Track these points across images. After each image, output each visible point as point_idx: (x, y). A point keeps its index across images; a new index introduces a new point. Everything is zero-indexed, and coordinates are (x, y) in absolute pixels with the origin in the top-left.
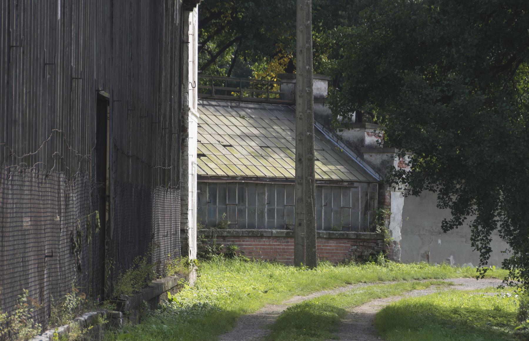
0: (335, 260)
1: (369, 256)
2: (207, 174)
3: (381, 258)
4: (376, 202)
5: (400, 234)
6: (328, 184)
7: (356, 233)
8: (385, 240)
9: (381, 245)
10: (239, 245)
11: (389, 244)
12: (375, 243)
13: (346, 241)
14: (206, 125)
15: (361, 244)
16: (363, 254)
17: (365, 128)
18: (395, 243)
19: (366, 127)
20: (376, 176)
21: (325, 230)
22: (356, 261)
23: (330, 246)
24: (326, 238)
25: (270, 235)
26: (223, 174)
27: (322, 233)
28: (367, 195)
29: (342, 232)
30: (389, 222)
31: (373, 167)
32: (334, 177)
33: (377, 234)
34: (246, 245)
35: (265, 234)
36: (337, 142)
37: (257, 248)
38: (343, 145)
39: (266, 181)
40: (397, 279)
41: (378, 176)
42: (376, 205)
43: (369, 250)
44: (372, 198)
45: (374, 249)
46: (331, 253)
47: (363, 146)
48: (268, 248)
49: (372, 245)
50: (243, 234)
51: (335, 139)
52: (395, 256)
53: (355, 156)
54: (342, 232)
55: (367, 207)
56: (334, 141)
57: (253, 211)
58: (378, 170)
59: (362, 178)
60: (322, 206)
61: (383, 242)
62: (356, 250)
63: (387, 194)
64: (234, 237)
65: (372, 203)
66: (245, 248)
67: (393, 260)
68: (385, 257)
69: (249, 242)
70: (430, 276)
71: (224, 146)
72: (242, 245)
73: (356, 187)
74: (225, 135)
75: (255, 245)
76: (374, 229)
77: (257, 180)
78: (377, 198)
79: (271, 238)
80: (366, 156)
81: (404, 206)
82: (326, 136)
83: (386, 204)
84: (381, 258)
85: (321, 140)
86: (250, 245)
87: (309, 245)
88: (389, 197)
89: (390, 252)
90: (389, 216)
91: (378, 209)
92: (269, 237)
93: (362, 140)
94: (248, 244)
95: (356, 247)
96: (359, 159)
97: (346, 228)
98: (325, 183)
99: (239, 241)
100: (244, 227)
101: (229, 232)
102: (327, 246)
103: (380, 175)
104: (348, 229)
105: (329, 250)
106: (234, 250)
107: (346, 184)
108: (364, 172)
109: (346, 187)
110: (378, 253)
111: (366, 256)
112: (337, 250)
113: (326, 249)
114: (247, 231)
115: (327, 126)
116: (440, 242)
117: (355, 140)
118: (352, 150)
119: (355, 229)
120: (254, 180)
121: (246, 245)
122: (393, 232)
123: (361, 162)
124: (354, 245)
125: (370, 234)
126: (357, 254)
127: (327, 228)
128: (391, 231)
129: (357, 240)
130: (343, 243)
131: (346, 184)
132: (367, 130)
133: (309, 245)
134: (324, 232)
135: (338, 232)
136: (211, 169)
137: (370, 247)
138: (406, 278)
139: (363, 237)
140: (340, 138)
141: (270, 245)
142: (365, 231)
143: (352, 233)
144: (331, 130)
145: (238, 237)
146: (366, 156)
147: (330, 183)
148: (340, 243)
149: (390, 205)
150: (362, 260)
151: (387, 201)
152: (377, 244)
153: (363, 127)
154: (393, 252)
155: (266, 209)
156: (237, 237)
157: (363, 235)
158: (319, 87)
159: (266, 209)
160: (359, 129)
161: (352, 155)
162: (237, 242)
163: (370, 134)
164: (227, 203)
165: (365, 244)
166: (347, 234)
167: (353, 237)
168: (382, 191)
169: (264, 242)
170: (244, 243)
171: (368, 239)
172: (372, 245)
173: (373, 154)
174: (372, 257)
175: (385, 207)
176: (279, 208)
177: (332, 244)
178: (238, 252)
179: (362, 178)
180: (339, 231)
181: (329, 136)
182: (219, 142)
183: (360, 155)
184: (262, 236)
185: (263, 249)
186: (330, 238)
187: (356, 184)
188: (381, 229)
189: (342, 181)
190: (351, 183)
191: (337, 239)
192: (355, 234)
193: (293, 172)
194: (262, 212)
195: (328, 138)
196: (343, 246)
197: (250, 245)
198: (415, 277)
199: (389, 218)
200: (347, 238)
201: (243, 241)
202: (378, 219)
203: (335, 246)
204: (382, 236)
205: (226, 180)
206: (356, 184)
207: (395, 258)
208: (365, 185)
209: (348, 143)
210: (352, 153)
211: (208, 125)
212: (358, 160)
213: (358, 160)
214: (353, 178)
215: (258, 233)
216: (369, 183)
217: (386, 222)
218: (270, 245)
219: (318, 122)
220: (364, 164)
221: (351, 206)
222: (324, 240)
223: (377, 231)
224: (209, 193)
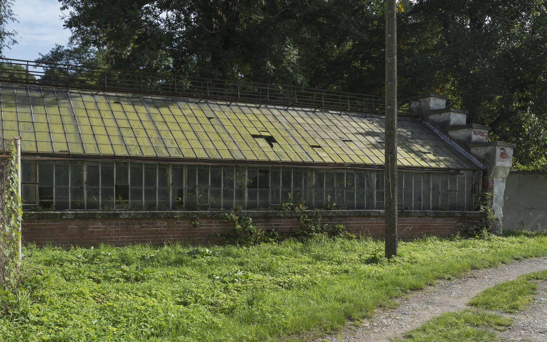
0: (442, 234)
1: (473, 231)
2: (314, 161)
3: (485, 232)
4: (481, 186)
5: (502, 212)
6: (435, 171)
7: (462, 212)
8: (488, 217)
9: (484, 221)
10: (344, 224)
11: (492, 221)
12: (479, 220)
13: (452, 219)
14: (335, 127)
15: (466, 221)
16: (468, 229)
17: (472, 128)
18: (497, 219)
19: (473, 127)
20: (481, 166)
21: (433, 209)
22: (462, 235)
23: (437, 223)
24: (433, 217)
25: (378, 215)
26: (331, 161)
27: (429, 212)
28: (472, 181)
29: (448, 211)
30: (492, 203)
31: (479, 159)
32: (442, 166)
33: (481, 213)
34: (353, 224)
35: (372, 214)
36: (450, 142)
37: (364, 226)
38: (454, 143)
39: (375, 168)
40: (494, 264)
41: (482, 166)
42: (480, 189)
43: (473, 226)
44: (477, 183)
45: (478, 225)
46: (438, 229)
47: (470, 143)
48: (376, 226)
49: (476, 221)
50: (349, 214)
51: (449, 139)
52: (497, 230)
53: (464, 151)
54: (448, 211)
55: (473, 190)
56: (448, 140)
57: (362, 194)
58: (482, 161)
59: (467, 167)
60: (430, 190)
61: (487, 219)
62: (462, 226)
63: (490, 180)
64: (341, 217)
65: (477, 187)
66: (352, 227)
67: (495, 233)
68: (488, 232)
69: (356, 221)
70: (530, 254)
71: (344, 141)
72: (350, 224)
73: (462, 174)
74: (349, 134)
75: (362, 223)
76: (478, 209)
77: (366, 167)
78: (481, 183)
79: (379, 217)
80: (473, 150)
81: (505, 190)
82: (441, 137)
83: (489, 188)
84: (485, 232)
85: (437, 140)
86: (358, 223)
87: (388, 230)
88: (492, 182)
89: (492, 227)
90: (492, 197)
91: (483, 192)
92: (377, 217)
93: (470, 138)
94: (354, 222)
95: (461, 224)
96: (467, 153)
97: (453, 207)
98: (433, 170)
99: (346, 221)
100: (353, 208)
101: (334, 212)
102: (435, 223)
103: (484, 165)
104: (455, 209)
105: (437, 226)
106: (339, 228)
107: (452, 171)
108: (470, 162)
109: (452, 174)
110: (482, 228)
111: (471, 231)
112: (444, 226)
113: (432, 226)
114: (354, 211)
115: (442, 130)
116: (531, 214)
117: (464, 138)
118: (461, 147)
119: (461, 208)
120: (361, 167)
121: (353, 224)
122: (496, 210)
123: (469, 155)
124: (460, 222)
125: (475, 213)
126: (462, 229)
127: (435, 208)
128: (494, 211)
129: (463, 217)
130: (450, 221)
131: (452, 171)
132: (474, 130)
133: (388, 230)
134: (432, 211)
135: (444, 211)
136: (320, 157)
137: (475, 224)
138: (506, 260)
139: (468, 215)
140: (451, 138)
141: (377, 223)
142: (470, 210)
143: (457, 213)
144: (446, 133)
145: (345, 217)
146: (473, 150)
147: (437, 171)
148: (447, 221)
149: (493, 188)
150: (467, 234)
151: (490, 185)
152: (481, 221)
153: (471, 127)
154: (495, 227)
155: (375, 192)
156: (344, 217)
157: (468, 213)
158: (438, 103)
159: (375, 192)
160: (467, 130)
161: (461, 150)
162: (343, 221)
163: (477, 132)
164: (335, 187)
165: (470, 221)
166: (453, 213)
167: (459, 215)
168: (485, 177)
169: (372, 220)
170: (351, 222)
171: (473, 217)
172: (476, 221)
173: (479, 148)
174: (477, 232)
175: (488, 190)
176: (110, 187)
177: (439, 221)
178: (343, 230)
179: (467, 167)
180: (446, 210)
181: (443, 137)
182: (340, 138)
183: (468, 149)
184: (369, 216)
185: (371, 226)
186: (437, 216)
187: (461, 172)
188: (484, 208)
189: (449, 169)
190: (458, 171)
191: (443, 217)
192: (460, 213)
193: (383, 159)
194: (371, 196)
195: (443, 139)
196: (449, 223)
197: (358, 223)
198: (516, 257)
199: (492, 199)
200: (453, 216)
201: (350, 220)
202: (482, 200)
203: (442, 223)
204: (485, 214)
205: (333, 166)
206: (461, 172)
207: (497, 232)
208: (471, 172)
209: (459, 142)
210: (461, 149)
211: (337, 126)
212: (466, 154)
213: (466, 154)
214: (460, 167)
215: (365, 213)
216: (474, 171)
217: (489, 203)
218: (377, 223)
219: (436, 128)
220: (471, 156)
221: (38, 182)
222: (431, 219)
223: (481, 210)
224: (316, 178)
